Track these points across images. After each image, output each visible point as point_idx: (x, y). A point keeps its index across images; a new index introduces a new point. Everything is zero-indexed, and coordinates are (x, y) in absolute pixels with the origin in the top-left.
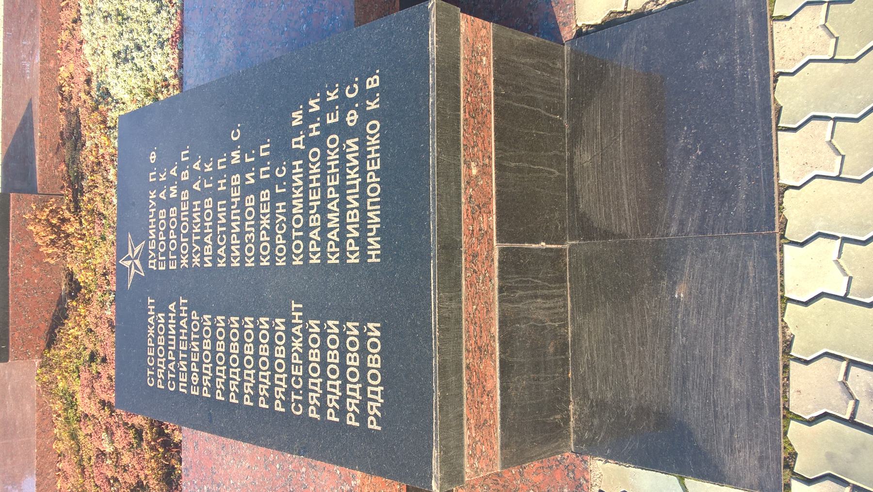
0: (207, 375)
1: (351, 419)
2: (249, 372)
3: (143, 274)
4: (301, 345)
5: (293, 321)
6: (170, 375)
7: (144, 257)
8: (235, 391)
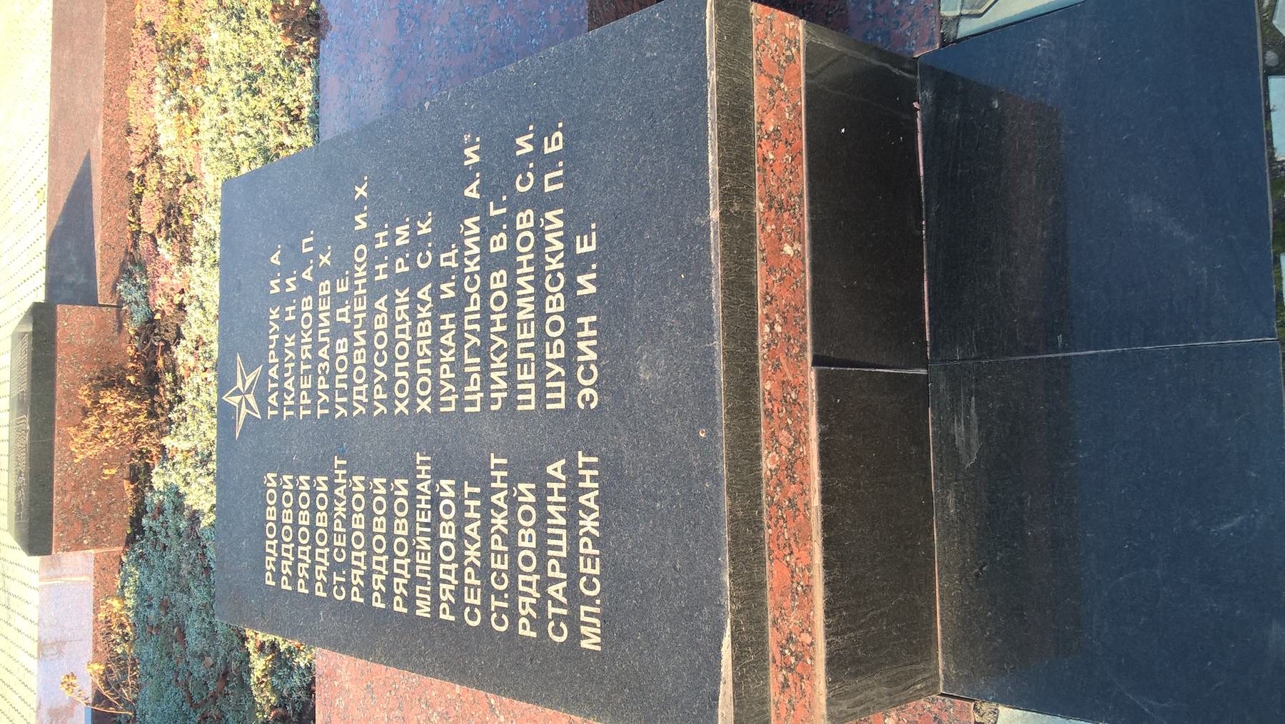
0: (402, 576)
1: (524, 627)
2: (448, 567)
3: (259, 416)
4: (506, 522)
5: (493, 485)
6: (551, 610)
7: (261, 393)
8: (380, 590)
